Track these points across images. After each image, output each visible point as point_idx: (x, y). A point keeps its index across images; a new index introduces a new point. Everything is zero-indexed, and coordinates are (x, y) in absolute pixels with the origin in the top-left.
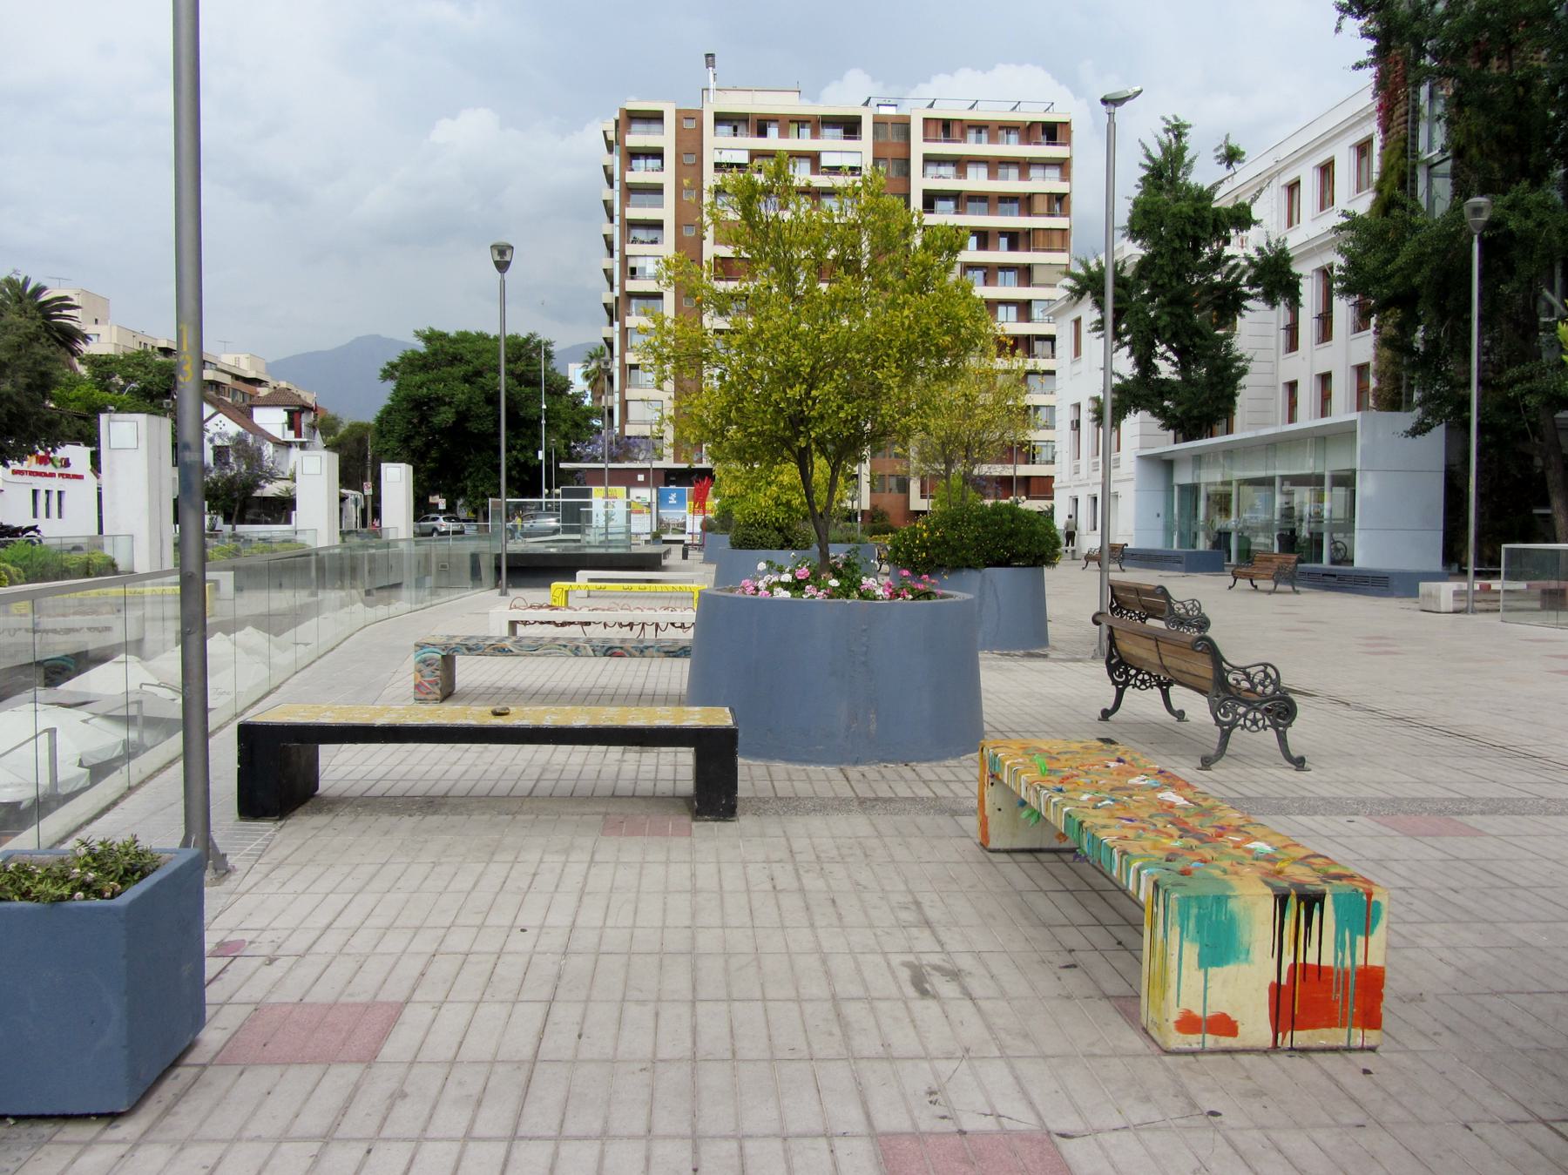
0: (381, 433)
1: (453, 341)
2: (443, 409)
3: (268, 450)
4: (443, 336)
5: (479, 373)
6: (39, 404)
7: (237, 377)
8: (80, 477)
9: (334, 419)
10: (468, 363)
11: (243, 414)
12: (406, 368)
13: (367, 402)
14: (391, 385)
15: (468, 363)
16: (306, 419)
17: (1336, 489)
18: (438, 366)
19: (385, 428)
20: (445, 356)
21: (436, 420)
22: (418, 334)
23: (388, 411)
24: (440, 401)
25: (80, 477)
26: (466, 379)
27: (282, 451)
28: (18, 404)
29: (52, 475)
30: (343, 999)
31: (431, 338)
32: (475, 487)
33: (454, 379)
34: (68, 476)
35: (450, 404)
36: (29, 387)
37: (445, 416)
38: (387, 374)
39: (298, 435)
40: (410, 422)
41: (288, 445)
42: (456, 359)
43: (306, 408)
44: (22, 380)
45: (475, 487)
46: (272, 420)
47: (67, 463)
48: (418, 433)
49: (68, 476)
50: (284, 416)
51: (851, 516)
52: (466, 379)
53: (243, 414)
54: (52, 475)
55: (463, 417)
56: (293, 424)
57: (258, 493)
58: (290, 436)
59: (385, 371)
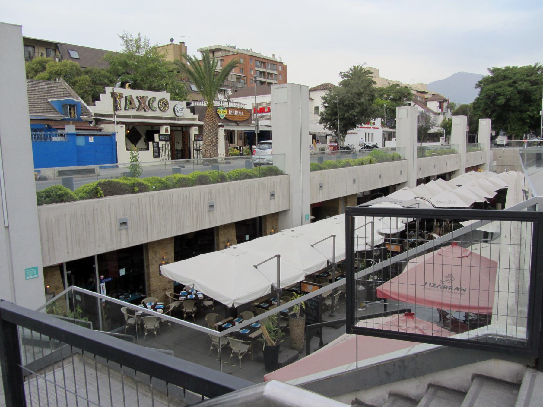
0: (475, 108)
1: (504, 71)
2: (500, 97)
3: (432, 116)
4: (499, 69)
5: (515, 82)
6: (370, 105)
7: (418, 92)
8: (378, 128)
9: (453, 104)
10: (510, 79)
11: (424, 104)
12: (484, 83)
13: (470, 95)
14: (479, 90)
15: (510, 79)
16: (445, 104)
17: (323, 319)
18: (498, 81)
19: (476, 106)
20: (500, 77)
21: (498, 102)
22: (489, 69)
23: (478, 99)
24: (499, 94)
25: (378, 128)
26: (510, 85)
27: (437, 116)
28: (366, 106)
29: (370, 128)
30: (71, 359)
31: (494, 71)
32: (511, 126)
33: (505, 85)
34: (374, 128)
35: (503, 95)
36: (369, 100)
37: (501, 101)
38: (478, 86)
39: (442, 110)
40: (487, 103)
41: (439, 114)
42: (505, 78)
43: (445, 100)
44: (367, 98)
45: (511, 126)
46: (433, 106)
47: (374, 124)
48: (489, 107)
49: (374, 128)
50: (438, 104)
51: (177, 150)
52: (510, 85)
53: (424, 104)
54: (370, 128)
55: (508, 100)
56: (441, 107)
57: (429, 131)
58: (439, 111)
59: (477, 84)
